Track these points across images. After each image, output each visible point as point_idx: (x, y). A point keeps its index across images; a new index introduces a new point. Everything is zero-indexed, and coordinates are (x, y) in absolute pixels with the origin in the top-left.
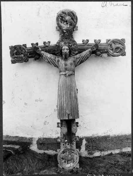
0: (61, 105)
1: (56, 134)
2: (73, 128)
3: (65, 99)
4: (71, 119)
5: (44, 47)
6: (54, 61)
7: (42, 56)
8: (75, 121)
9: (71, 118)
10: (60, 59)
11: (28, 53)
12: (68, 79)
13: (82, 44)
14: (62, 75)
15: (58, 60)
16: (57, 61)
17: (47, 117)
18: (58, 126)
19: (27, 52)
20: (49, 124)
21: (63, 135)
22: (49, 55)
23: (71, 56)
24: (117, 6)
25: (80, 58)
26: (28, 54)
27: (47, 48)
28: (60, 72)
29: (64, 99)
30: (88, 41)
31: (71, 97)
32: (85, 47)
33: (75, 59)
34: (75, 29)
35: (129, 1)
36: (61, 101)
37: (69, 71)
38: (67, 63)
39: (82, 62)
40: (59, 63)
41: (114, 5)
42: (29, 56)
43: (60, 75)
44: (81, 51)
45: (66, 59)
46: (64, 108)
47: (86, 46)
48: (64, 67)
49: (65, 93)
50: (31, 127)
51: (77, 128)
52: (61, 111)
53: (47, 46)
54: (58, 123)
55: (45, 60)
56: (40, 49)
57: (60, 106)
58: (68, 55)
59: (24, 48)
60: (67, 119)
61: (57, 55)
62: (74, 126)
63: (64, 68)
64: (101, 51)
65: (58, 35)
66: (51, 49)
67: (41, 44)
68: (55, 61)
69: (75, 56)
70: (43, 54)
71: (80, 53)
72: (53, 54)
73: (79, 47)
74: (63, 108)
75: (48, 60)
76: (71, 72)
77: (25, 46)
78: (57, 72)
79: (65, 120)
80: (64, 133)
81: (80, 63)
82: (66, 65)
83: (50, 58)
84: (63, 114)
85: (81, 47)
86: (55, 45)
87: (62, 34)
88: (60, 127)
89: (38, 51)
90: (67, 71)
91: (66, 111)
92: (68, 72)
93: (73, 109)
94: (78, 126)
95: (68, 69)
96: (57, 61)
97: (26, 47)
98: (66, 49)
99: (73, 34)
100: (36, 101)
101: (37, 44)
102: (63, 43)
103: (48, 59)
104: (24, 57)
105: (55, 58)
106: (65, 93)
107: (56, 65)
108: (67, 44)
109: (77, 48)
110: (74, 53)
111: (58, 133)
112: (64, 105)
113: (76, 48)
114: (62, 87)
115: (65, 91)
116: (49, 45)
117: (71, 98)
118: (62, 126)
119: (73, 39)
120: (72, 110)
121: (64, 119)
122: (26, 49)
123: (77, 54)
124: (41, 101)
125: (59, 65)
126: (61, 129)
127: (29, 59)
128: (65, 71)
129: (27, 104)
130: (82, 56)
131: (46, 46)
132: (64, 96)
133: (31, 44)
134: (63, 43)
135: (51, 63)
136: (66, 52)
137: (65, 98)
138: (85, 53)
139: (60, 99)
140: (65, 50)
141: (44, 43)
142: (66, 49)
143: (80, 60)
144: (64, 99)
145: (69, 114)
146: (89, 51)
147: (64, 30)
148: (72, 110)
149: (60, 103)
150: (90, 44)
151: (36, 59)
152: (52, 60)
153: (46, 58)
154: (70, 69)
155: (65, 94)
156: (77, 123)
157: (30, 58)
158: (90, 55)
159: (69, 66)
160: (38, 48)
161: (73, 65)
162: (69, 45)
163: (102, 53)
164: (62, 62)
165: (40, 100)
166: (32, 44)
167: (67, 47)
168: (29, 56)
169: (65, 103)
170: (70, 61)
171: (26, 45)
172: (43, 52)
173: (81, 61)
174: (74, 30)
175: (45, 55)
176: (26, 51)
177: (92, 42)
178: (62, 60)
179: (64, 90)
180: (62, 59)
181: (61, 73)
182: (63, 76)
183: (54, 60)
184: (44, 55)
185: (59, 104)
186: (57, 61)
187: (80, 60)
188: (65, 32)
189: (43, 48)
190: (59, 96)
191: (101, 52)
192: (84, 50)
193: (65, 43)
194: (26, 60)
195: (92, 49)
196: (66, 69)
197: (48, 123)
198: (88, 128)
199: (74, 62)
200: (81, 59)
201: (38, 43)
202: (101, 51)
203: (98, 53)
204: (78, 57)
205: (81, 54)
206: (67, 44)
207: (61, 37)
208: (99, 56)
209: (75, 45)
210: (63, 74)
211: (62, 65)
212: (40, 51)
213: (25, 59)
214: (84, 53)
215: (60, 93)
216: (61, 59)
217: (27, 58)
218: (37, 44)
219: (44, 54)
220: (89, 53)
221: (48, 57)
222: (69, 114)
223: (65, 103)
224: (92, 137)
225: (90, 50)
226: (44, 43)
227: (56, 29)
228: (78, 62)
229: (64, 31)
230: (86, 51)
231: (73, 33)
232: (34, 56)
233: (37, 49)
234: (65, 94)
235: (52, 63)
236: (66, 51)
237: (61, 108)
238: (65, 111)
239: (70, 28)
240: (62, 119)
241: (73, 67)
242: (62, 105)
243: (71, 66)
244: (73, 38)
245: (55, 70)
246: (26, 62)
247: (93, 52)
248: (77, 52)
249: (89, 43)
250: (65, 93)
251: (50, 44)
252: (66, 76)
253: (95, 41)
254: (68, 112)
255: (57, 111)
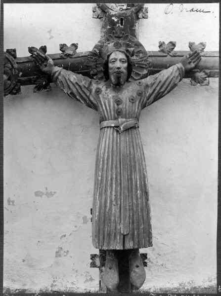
0: (102, 211)
1: (87, 280)
2: (135, 272)
3: (114, 193)
4: (128, 250)
5: (62, 58)
6: (86, 91)
7: (54, 79)
8: (139, 252)
9: (129, 245)
10: (102, 86)
11: (20, 70)
12: (124, 139)
13: (159, 51)
14: (108, 127)
15: (98, 88)
16: (94, 91)
17: (65, 236)
18: (93, 265)
19: (18, 69)
20: (68, 255)
21: (105, 288)
22: (73, 77)
23: (130, 82)
24: (192, 12)
25: (156, 85)
26: (21, 73)
27: (68, 59)
28: (103, 119)
29: (112, 193)
30: (173, 45)
31: (132, 188)
32: (165, 59)
33: (143, 87)
34: (140, 15)
35: (216, 2)
36: (104, 197)
37: (126, 118)
38: (120, 96)
39: (159, 96)
40: (100, 96)
41: (188, 10)
42: (23, 79)
43: (101, 129)
44: (155, 69)
45: (118, 86)
46: (113, 218)
47: (169, 57)
48: (114, 107)
49: (116, 175)
50: (24, 261)
51: (144, 271)
52: (101, 232)
53: (69, 55)
54: (93, 257)
55: (62, 90)
56: (51, 61)
57: (100, 212)
58: (123, 77)
59: (11, 58)
60: (119, 247)
61: (95, 78)
62: (137, 267)
63: (114, 110)
64: (208, 71)
65: (99, 28)
66: (79, 63)
67: (53, 50)
68: (90, 91)
69: (143, 80)
70: (57, 74)
71: (152, 73)
72: (83, 75)
73: (150, 60)
74: (110, 220)
75: (70, 89)
76: (131, 122)
77: (13, 53)
78: (93, 123)
79: (115, 252)
80: (110, 287)
81: (155, 100)
82: (118, 102)
83: (77, 83)
84: (109, 235)
85: (153, 58)
86: (90, 52)
87: (109, 27)
88: (99, 267)
89: (46, 66)
90: (122, 118)
91: (118, 227)
92: (124, 120)
93: (135, 221)
94: (145, 264)
95: (124, 113)
96: (96, 90)
97: (15, 57)
98: (120, 60)
99: (136, 28)
100: (37, 194)
101: (44, 49)
102: (111, 45)
103: (71, 85)
104: (9, 82)
105: (90, 83)
106: (116, 178)
107: (92, 103)
108: (123, 49)
109: (146, 60)
110: (138, 74)
111: (91, 279)
112: (110, 209)
113: (143, 62)
114: (108, 160)
115: (114, 171)
116: (75, 52)
117: (132, 191)
118: (103, 265)
119: (136, 40)
120: (133, 223)
121: (112, 248)
122: (16, 61)
123: (145, 76)
124: (50, 194)
125: (100, 101)
126: (101, 271)
127: (23, 88)
128: (116, 119)
129: (13, 202)
130: (160, 82)
131: (66, 55)
132: (112, 184)
133: (29, 48)
134: (111, 45)
135: (77, 97)
136: (119, 68)
137: (116, 188)
138: (169, 74)
139: (101, 194)
140: (118, 62)
141: (63, 47)
142: (120, 60)
143: (156, 91)
144: (111, 193)
145: (124, 236)
146: (178, 69)
147: (113, 16)
148: (133, 223)
149: (101, 203)
150: (180, 52)
151: (39, 88)
152: (81, 88)
153: (64, 82)
154: (129, 114)
155: (114, 180)
156: (144, 256)
157: (24, 83)
158: (180, 80)
159: (126, 105)
160: (46, 59)
161: (137, 102)
162: (127, 51)
163: (209, 77)
164: (107, 96)
165: (47, 193)
166: (31, 50)
167: (121, 56)
168: (23, 79)
169: (114, 203)
170: (129, 92)
171: (14, 51)
172: (57, 69)
173: (159, 93)
174: (140, 17)
175: (63, 76)
176: (16, 66)
177: (182, 47)
178: (109, 90)
179: (112, 168)
180: (108, 87)
181: (105, 124)
182: (109, 132)
183: (87, 89)
184: (60, 77)
185: (98, 206)
186: (94, 91)
187: (156, 91)
188: (116, 20)
189: (60, 61)
190: (100, 186)
191: (206, 74)
192: (166, 67)
193: (117, 46)
194: (13, 89)
195: (184, 63)
196: (119, 113)
197: (68, 251)
198: (169, 266)
199: (140, 94)
200: (158, 88)
201: (45, 47)
202: (208, 71)
203: (200, 75)
204: (149, 84)
205: (157, 75)
206: (123, 49)
207: (106, 33)
208: (202, 82)
209: (141, 55)
210: (109, 125)
211: (106, 101)
212: (51, 66)
213: (12, 86)
214: (165, 74)
215: (102, 177)
216: (105, 87)
217: (16, 85)
218: (44, 49)
219: (60, 73)
220: (177, 74)
221: (72, 80)
222: (124, 236)
223: (114, 203)
224: (178, 289)
225: (180, 65)
226: (63, 47)
227: (92, 13)
228: (150, 95)
229: (113, 18)
230: (170, 69)
231: (137, 24)
232: (35, 81)
233: (43, 62)
234: (114, 180)
235: (81, 97)
236: (118, 64)
237: (104, 216)
238: (116, 226)
239: (129, 13)
240: (105, 248)
241: (136, 107)
242: (107, 210)
243: (131, 104)
244: (135, 37)
245: (85, 118)
246: (15, 94)
247: (189, 73)
248: (145, 72)
249: (176, 49)
250: (114, 176)
251: (78, 51)
252: (117, 131)
253: (191, 45)
254: (122, 229)
255: (90, 224)
